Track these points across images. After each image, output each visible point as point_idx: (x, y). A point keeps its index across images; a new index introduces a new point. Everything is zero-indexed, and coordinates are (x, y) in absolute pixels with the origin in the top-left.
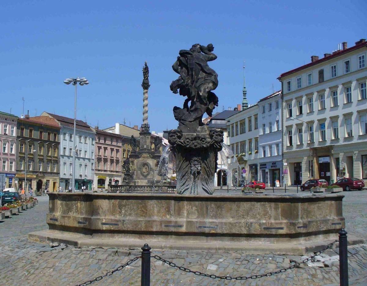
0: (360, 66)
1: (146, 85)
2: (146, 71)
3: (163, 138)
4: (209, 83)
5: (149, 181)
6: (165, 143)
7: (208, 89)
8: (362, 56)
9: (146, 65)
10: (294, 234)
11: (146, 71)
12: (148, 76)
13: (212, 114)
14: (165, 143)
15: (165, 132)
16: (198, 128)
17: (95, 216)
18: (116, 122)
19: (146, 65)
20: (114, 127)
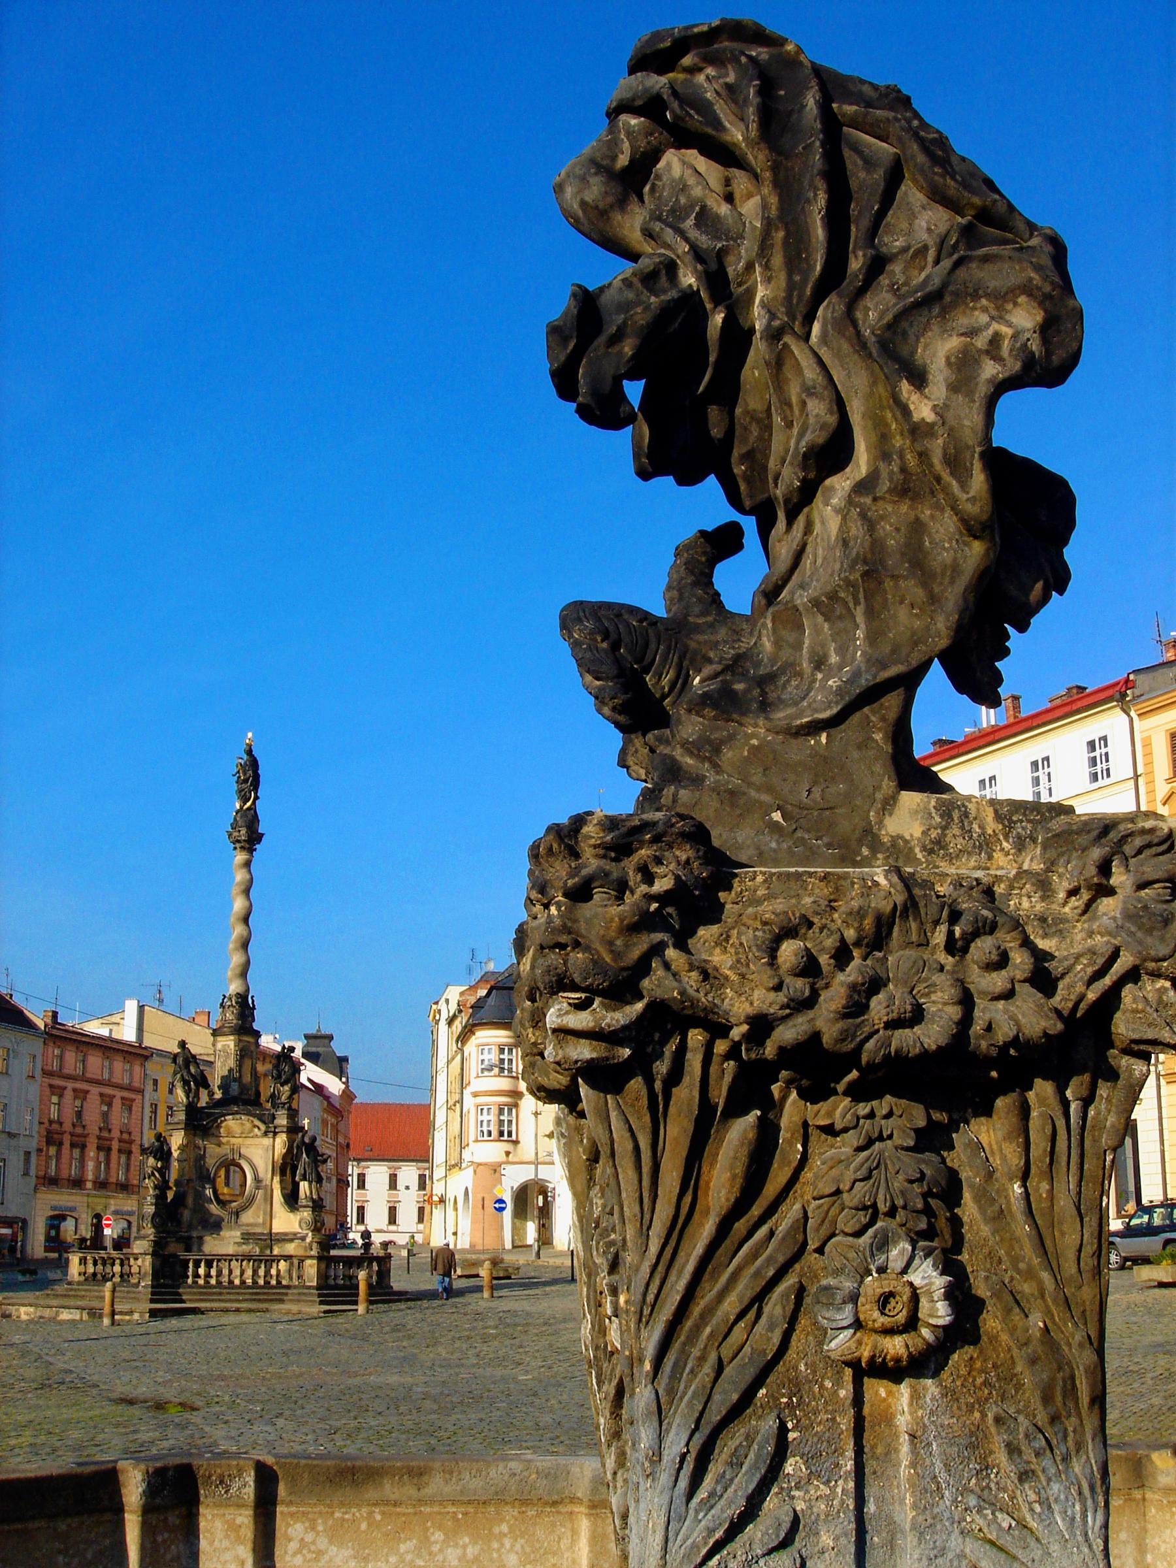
0: (1094, 777)
1: (250, 835)
2: (250, 776)
3: (302, 1060)
4: (1002, 299)
5: (247, 1237)
6: (310, 1080)
7: (997, 358)
8: (1043, 760)
9: (249, 752)
10: (739, 1400)
11: (250, 776)
12: (257, 798)
13: (998, 679)
14: (310, 1080)
15: (307, 1037)
16: (889, 804)
17: (767, 457)
18: (130, 997)
19: (249, 752)
20: (120, 1016)
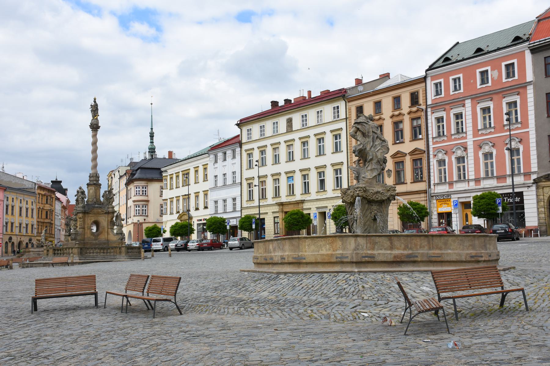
9: (95, 102)
11: (95, 109)
